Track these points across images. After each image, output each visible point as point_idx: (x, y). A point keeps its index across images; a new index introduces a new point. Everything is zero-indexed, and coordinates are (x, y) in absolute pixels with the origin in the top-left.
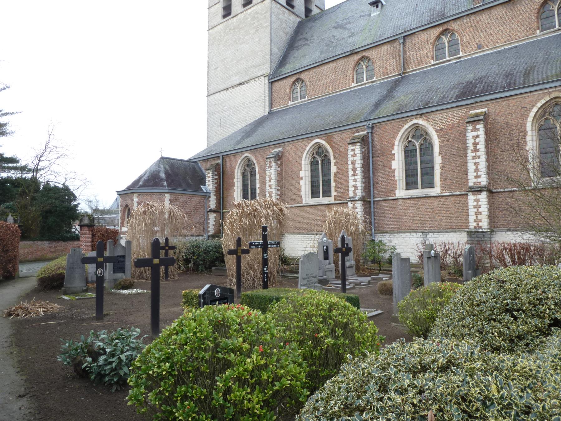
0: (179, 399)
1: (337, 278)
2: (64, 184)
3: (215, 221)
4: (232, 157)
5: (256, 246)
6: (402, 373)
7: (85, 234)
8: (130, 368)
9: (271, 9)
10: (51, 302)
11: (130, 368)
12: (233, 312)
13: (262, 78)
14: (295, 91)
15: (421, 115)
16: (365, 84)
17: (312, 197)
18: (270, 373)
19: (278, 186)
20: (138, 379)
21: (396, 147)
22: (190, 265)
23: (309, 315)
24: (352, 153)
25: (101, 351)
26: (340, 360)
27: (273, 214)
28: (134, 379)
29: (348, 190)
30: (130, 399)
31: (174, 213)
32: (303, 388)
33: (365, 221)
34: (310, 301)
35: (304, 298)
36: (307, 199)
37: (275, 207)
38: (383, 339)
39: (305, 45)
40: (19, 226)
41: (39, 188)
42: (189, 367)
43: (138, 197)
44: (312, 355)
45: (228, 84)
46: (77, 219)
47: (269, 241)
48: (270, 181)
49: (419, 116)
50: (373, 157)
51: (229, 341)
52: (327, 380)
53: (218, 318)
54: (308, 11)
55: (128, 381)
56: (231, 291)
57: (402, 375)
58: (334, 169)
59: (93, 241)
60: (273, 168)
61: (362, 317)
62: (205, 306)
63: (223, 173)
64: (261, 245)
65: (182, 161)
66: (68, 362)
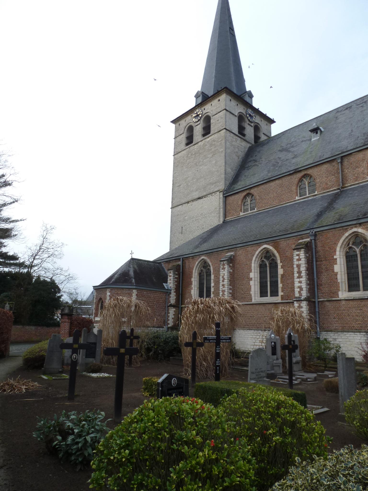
0: (135, 486)
1: (284, 373)
2: (51, 279)
3: (174, 315)
4: (191, 259)
5: (209, 340)
6: (351, 483)
7: (65, 322)
8: (94, 452)
9: (225, 138)
10: (32, 381)
11: (94, 452)
12: (188, 404)
13: (218, 193)
14: (246, 204)
16: (308, 197)
17: (261, 296)
18: (221, 468)
19: (230, 285)
20: (100, 462)
21: (338, 253)
22: (151, 353)
23: (258, 412)
24: (297, 257)
25: (70, 431)
26: (288, 462)
27: (226, 311)
28: (96, 462)
29: (294, 290)
30: (92, 483)
31: (139, 307)
32: (252, 486)
33: (310, 320)
34: (259, 398)
35: (253, 395)
36: (256, 298)
37: (227, 305)
38: (331, 441)
39: (254, 166)
40: (13, 313)
41: (32, 281)
42: (146, 456)
43: (110, 292)
44: (260, 451)
45: (189, 198)
46: (59, 309)
47: (222, 336)
48: (223, 281)
49: (358, 225)
50: (316, 261)
51: (184, 433)
52: (276, 482)
53: (174, 410)
54: (257, 138)
55: (91, 463)
56: (187, 381)
57: (351, 486)
58: (280, 271)
59: (70, 328)
60: (226, 270)
61: (309, 417)
62: (163, 398)
63: (182, 273)
64: (215, 339)
66: (41, 439)
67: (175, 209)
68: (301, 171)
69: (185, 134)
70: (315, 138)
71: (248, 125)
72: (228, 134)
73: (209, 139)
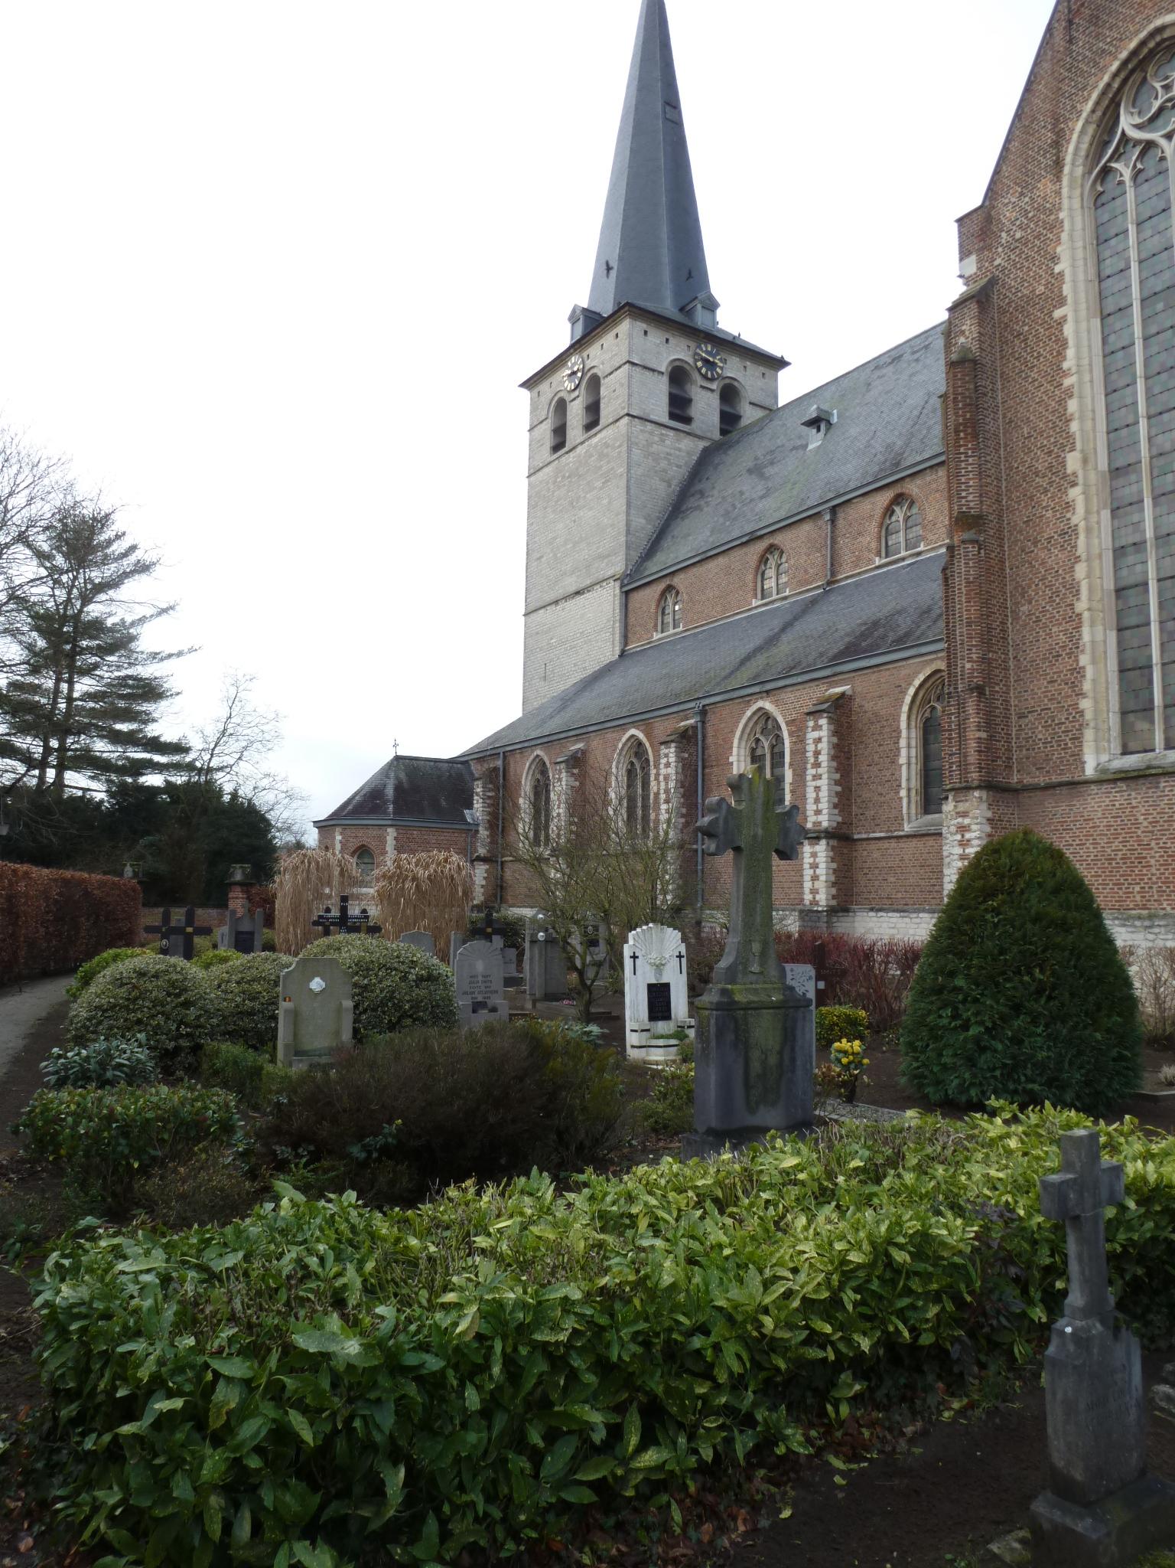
15: (767, 692)
21: (735, 750)
65: (436, 761)
67: (534, 616)
68: (761, 537)
69: (549, 420)
70: (815, 440)
71: (699, 390)
72: (638, 425)
73: (603, 436)
